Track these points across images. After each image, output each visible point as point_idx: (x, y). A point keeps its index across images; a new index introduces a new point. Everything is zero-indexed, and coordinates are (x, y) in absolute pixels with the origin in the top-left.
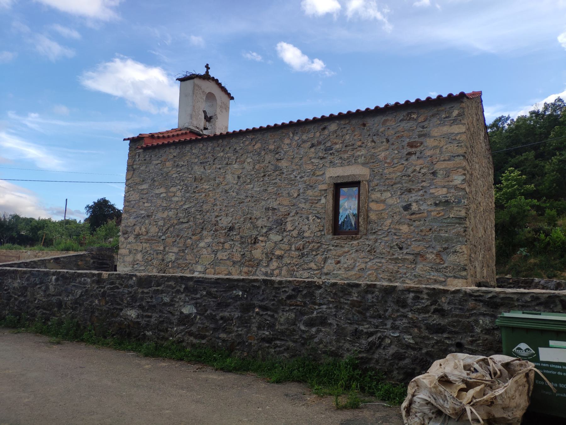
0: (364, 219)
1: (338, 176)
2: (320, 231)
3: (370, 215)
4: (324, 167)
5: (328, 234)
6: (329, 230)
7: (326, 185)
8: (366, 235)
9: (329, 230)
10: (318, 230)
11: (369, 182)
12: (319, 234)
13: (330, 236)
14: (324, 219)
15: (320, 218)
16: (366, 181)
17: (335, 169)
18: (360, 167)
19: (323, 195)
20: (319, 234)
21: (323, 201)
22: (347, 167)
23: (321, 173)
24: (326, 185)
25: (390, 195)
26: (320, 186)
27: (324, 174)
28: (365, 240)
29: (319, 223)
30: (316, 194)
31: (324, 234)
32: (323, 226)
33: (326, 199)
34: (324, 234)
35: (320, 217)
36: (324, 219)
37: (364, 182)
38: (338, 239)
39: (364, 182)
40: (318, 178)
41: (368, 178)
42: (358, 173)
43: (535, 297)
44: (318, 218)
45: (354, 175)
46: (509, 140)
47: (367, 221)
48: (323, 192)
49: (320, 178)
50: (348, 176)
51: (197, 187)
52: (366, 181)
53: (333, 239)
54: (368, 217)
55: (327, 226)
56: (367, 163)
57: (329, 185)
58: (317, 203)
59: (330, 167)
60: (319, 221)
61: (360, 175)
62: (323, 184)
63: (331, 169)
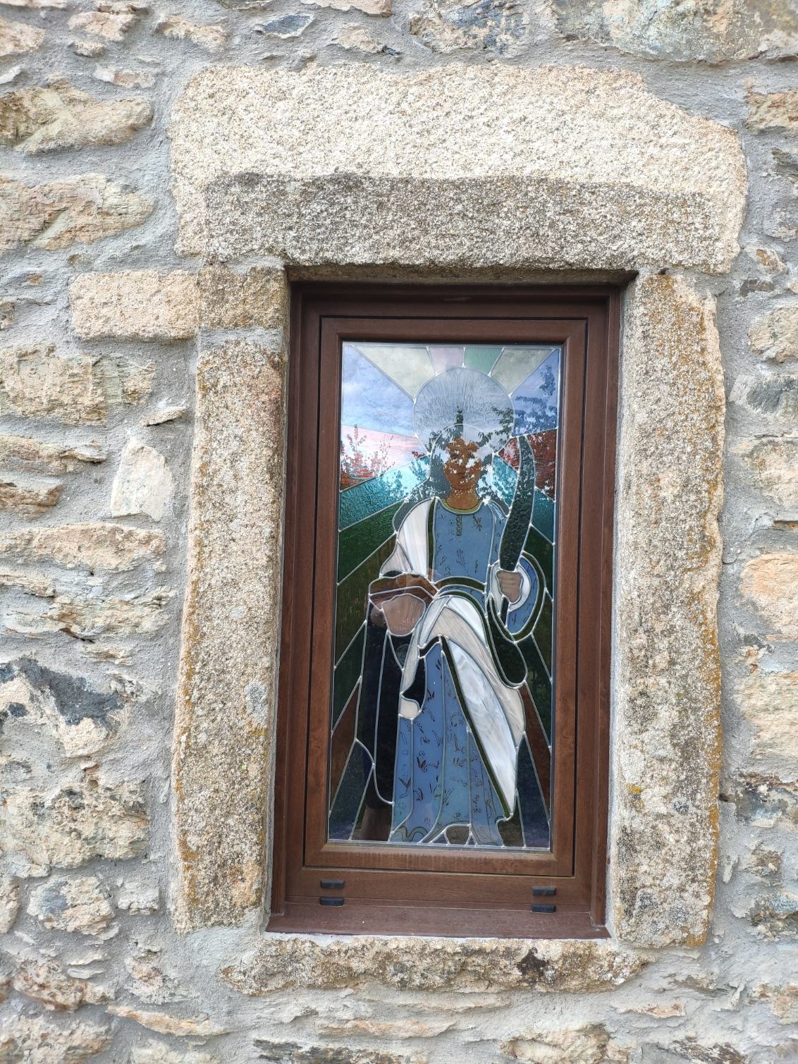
0: (688, 750)
1: (348, 183)
2: (94, 862)
3: (750, 696)
4: (146, 52)
5: (209, 909)
6: (226, 871)
7: (179, 284)
8: (704, 944)
9: (226, 871)
10: (74, 853)
11: (736, 288)
12: (86, 903)
13: (242, 944)
14: (158, 710)
15: (99, 707)
16: (706, 275)
17: (298, 83)
18: (632, 100)
19: (134, 401)
20: (86, 903)
21: (140, 479)
22: (465, 81)
23: (108, 117)
24: (179, 284)
25: (80, 400)
26: (90, 288)
27: (141, 132)
28: (690, 1002)
29: (92, 764)
30: (44, 383)
31: (159, 913)
32: (137, 811)
33: (176, 455)
34: (159, 913)
35: (98, 681)
36: (158, 710)
37: (685, 291)
38: (338, 977)
39: (685, 291)
40: (64, 178)
41: (727, 242)
42: (605, 172)
43: (195, 1040)
44: (70, 696)
45: (558, 188)
46: (323, 27)
47: (721, 773)
48: (138, 372)
49: (96, 182)
50: (485, 196)
51: (275, 156)
52: (706, 275)
53: (275, 975)
54: (728, 719)
55: (184, 820)
56: (717, 66)
57: (218, 278)
58: (51, 504)
59: (225, 54)
60: (86, 735)
61: (627, 199)
62: (137, 258)
63: (245, 76)
